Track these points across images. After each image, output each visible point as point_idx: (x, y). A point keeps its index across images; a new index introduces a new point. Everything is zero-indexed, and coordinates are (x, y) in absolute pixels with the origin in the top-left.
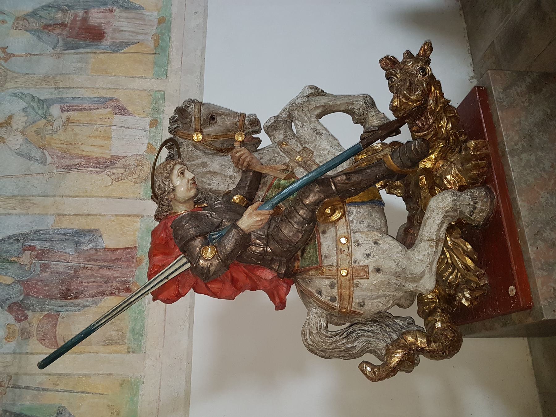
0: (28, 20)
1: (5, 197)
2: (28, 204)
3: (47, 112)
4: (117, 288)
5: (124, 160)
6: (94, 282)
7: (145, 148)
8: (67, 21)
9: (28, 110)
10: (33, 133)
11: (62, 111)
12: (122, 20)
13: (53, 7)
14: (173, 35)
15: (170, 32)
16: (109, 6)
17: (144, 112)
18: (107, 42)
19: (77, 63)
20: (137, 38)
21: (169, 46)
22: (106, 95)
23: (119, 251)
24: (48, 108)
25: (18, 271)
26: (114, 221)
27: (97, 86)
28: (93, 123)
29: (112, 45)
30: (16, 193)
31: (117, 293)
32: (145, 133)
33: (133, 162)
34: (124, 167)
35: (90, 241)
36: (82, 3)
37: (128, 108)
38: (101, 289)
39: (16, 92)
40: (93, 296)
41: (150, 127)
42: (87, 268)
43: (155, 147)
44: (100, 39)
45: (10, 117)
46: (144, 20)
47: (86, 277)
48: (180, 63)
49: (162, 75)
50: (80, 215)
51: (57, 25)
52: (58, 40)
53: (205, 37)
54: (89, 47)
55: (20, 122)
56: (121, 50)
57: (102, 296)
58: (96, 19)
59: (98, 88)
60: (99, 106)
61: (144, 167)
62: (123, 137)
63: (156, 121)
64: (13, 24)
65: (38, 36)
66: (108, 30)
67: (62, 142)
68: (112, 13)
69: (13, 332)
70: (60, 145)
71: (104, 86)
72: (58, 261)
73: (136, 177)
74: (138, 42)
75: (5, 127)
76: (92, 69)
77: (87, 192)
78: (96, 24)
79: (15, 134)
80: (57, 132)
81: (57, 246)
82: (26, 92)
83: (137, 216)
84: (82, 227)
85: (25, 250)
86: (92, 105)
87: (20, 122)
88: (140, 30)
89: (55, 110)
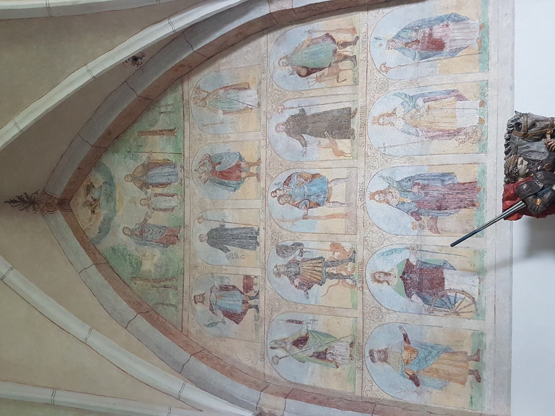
2: (413, 160)
5: (465, 130)
6: (454, 201)
7: (477, 121)
8: (419, 38)
10: (409, 118)
11: (424, 102)
12: (456, 31)
13: (409, 29)
14: (491, 36)
18: (447, 50)
20: (466, 44)
21: (489, 45)
23: (467, 184)
28: (444, 108)
29: (450, 52)
30: (405, 154)
32: (477, 111)
33: (470, 130)
34: (466, 134)
35: (450, 179)
38: (459, 205)
44: (442, 49)
45: (395, 110)
46: (470, 28)
48: (497, 58)
50: (442, 165)
53: (514, 34)
56: (457, 54)
58: (438, 34)
59: (444, 84)
61: (478, 133)
62: (464, 115)
64: (387, 45)
65: (403, 52)
66: (446, 41)
67: (427, 122)
68: (448, 27)
69: (416, 226)
70: (425, 124)
71: (448, 83)
75: (393, 116)
78: (438, 37)
83: (475, 163)
85: (414, 185)
86: (442, 96)
89: (420, 102)
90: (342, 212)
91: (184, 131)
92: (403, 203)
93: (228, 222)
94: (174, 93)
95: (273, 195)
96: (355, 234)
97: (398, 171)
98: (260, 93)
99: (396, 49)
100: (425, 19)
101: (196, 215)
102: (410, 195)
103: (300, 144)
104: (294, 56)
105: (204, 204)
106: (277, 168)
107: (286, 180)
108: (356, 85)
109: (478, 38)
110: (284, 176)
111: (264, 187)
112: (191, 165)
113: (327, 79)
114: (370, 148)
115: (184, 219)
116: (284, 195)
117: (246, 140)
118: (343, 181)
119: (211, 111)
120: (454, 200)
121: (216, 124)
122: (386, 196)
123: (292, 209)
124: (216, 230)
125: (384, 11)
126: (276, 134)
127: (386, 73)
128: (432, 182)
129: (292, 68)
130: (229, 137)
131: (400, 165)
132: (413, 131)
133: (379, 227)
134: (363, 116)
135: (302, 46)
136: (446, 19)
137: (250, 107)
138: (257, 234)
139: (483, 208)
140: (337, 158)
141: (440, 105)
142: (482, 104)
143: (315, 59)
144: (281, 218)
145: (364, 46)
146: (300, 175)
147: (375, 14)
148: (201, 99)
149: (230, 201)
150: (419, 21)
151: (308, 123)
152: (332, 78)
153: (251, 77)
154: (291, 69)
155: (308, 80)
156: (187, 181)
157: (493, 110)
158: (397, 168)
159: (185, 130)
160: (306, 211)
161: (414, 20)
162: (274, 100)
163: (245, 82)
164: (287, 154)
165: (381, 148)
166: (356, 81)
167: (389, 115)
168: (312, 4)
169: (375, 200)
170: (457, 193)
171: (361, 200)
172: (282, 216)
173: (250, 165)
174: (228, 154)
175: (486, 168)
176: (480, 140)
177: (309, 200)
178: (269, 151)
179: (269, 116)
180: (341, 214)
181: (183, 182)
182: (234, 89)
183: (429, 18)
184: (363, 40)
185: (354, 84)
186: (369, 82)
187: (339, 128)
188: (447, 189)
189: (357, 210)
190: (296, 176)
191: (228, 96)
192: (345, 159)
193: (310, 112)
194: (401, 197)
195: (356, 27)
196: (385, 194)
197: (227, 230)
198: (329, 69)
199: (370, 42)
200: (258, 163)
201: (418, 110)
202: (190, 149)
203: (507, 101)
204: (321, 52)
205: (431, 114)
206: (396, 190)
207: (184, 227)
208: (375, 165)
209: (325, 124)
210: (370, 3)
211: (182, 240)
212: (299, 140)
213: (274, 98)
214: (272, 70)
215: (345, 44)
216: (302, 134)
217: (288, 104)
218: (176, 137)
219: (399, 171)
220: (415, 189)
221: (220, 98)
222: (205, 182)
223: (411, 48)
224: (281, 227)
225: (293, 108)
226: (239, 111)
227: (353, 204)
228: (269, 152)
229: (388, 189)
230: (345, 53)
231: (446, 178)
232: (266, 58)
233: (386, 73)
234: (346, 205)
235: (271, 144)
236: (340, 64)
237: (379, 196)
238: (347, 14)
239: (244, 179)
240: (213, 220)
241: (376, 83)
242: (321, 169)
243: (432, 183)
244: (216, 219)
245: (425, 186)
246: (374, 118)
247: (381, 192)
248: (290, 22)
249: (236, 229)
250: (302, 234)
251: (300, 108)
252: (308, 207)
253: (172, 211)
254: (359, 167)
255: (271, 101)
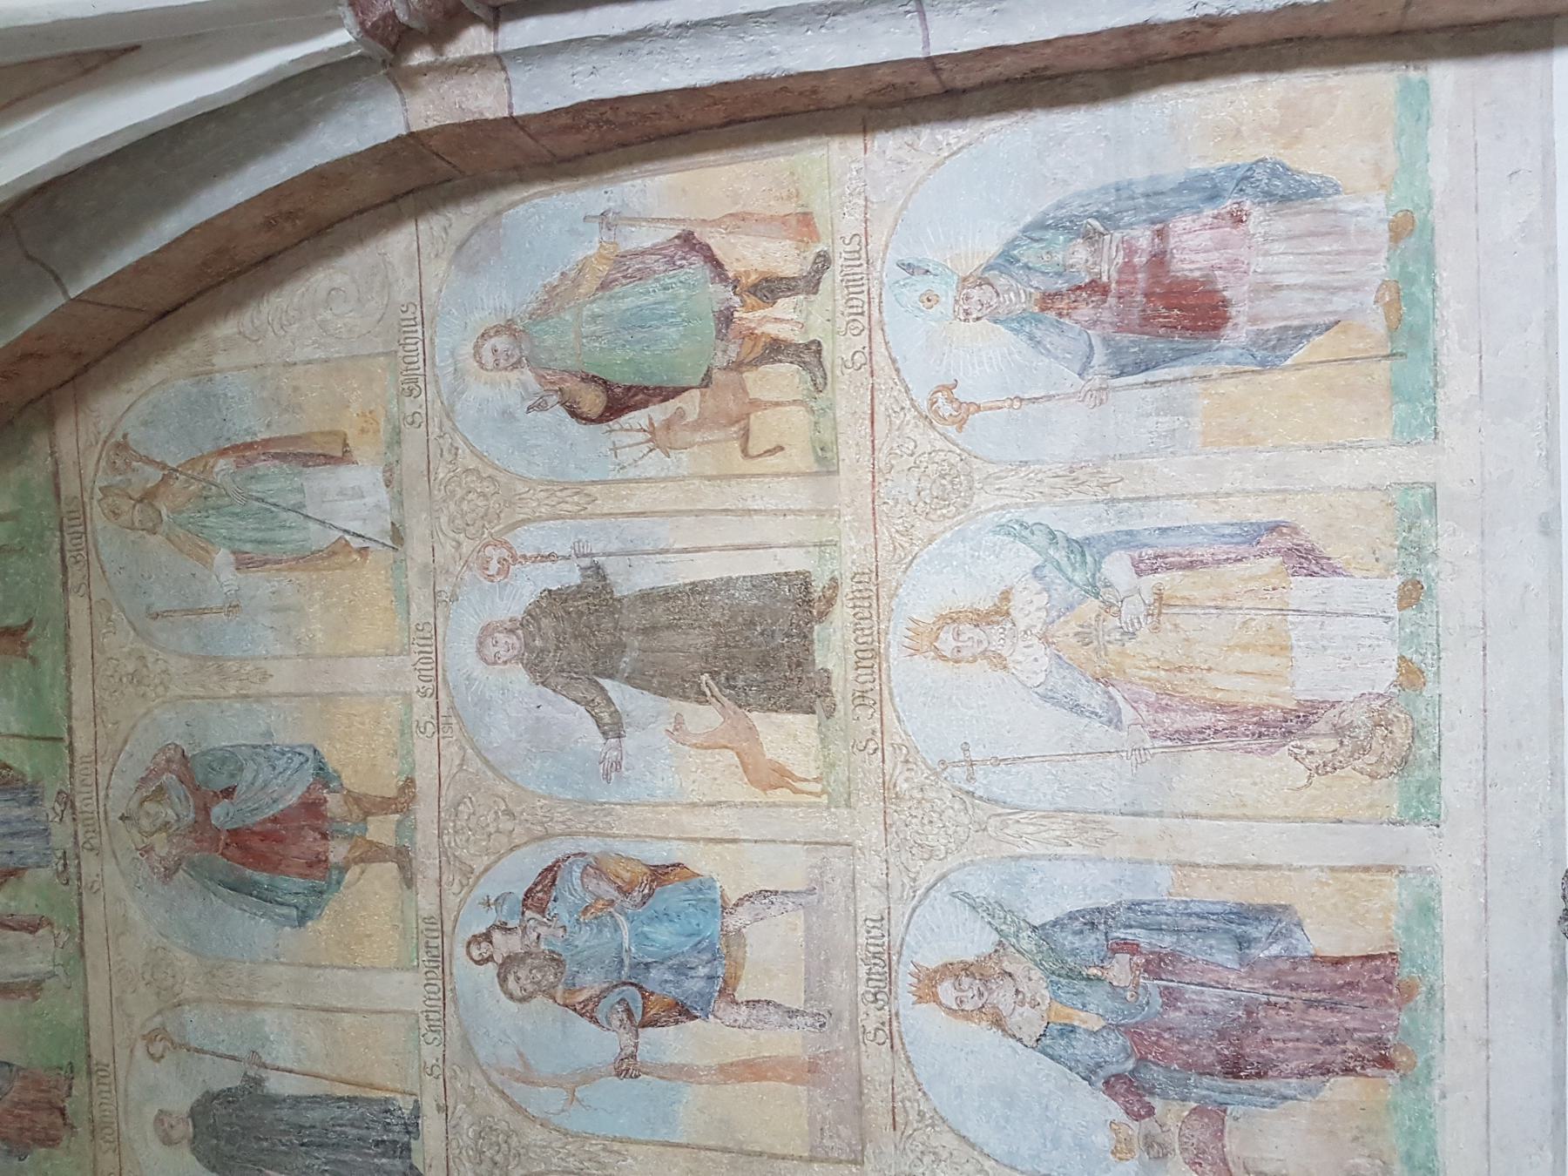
0: (992, 281)
1: (1038, 814)
2: (1099, 834)
3: (1098, 575)
4: (1358, 1057)
5: (1335, 711)
6: (1298, 1040)
7: (1391, 674)
8: (1107, 271)
9: (1046, 571)
10: (1073, 641)
11: (1139, 573)
12: (1278, 247)
13: (1056, 227)
14: (1444, 276)
15: (1435, 266)
16: (1230, 202)
17: (1377, 560)
18: (1237, 334)
19: (1158, 415)
20: (1330, 308)
21: (1435, 320)
22: (1258, 515)
23: (1352, 964)
24: (1097, 564)
25: (1109, 1002)
26: (1329, 885)
27: (1227, 486)
28: (1232, 604)
29: (1254, 343)
30: (1063, 804)
31: (1358, 1069)
32: (1386, 628)
33: (1359, 716)
34: (1338, 731)
35: (1274, 937)
36: (1142, 200)
37: (1328, 552)
38: (1319, 1059)
39: (1004, 521)
40: (1302, 1075)
41: (1401, 609)
42: (1275, 1004)
43: (1420, 670)
44: (1216, 328)
45: (1006, 596)
46: (1344, 233)
47: (1277, 1027)
48: (1476, 380)
49: (1422, 427)
50: (1237, 867)
51: (1078, 292)
52: (1091, 344)
53: (1552, 270)
54: (1185, 360)
55: (1033, 609)
56: (1286, 358)
57: (1322, 1074)
58: (1193, 257)
59: (1228, 495)
60: (1243, 549)
61: (1394, 729)
62: (1325, 643)
63: (1417, 584)
64: (956, 302)
65: (1031, 338)
66: (1235, 291)
67: (1154, 663)
68: (1242, 227)
69: (1128, 1141)
70: (1148, 673)
71: (1249, 487)
72: (1202, 985)
73: (1374, 759)
74: (1337, 323)
75: (998, 623)
76: (1203, 433)
77: (1244, 805)
78: (1197, 274)
79: (1026, 643)
80: (1134, 634)
81: (1190, 945)
82: (1030, 520)
83: (1388, 869)
84: (1247, 899)
85: (1115, 952)
86: (1221, 550)
87: (1033, 609)
88: (1336, 277)
89: (1117, 568)
90: (792, 1053)
91: (67, 636)
92: (1068, 1031)
93: (278, 1069)
94: (19, 463)
95: (475, 953)
96: (855, 1162)
97: (1034, 879)
98: (401, 483)
99: (1001, 322)
100: (1130, 183)
101: (138, 1021)
102: (1097, 997)
103: (591, 721)
104: (543, 326)
105: (169, 971)
106: (492, 829)
107: (536, 884)
108: (829, 473)
109: (1384, 282)
110: (522, 869)
111: (436, 913)
112: (102, 794)
113: (698, 438)
114: (907, 761)
115: (88, 1035)
116: (529, 954)
117: (343, 694)
118: (790, 906)
119: (181, 551)
120: (1298, 1035)
121: (203, 612)
122: (991, 991)
123: (564, 1024)
124: (226, 1097)
125: (939, 137)
126: (479, 670)
127: (960, 429)
128: (1194, 941)
129: (540, 378)
130: (265, 676)
131: (1041, 850)
132: (1093, 697)
133: (964, 1133)
134: (867, 615)
135: (576, 284)
136: (1230, 186)
137: (356, 543)
138: (408, 1133)
139: (1429, 1080)
140: (758, 796)
141: (1212, 592)
142: (1413, 594)
143: (638, 347)
144: (519, 1067)
145: (855, 303)
146: (597, 868)
147: (900, 153)
148: (137, 496)
149: (282, 968)
150: (1104, 189)
151: (622, 629)
152: (718, 434)
153: (355, 408)
154: (535, 386)
155: (614, 437)
156: (90, 866)
157: (1462, 627)
158: (1032, 864)
159: (72, 633)
160: (627, 1039)
161: (1079, 185)
162: (463, 515)
163: (327, 429)
164: (536, 766)
165: (954, 764)
166: (829, 455)
167: (982, 619)
168: (602, 102)
169: (940, 1004)
170: (1310, 1004)
171: (876, 1000)
172: (521, 1055)
173: (369, 807)
174: (264, 750)
175: (1439, 893)
176: (1405, 760)
177: (640, 988)
178: (455, 749)
179: (445, 587)
180: (788, 1062)
181: (72, 870)
182: (282, 457)
183: (1151, 178)
184: (848, 270)
185: (815, 468)
186: (882, 465)
187: (763, 663)
188: (1263, 980)
189: (863, 1048)
190: (577, 872)
191: (256, 488)
192: (796, 805)
193: (632, 579)
194: (1056, 1005)
195: (816, 208)
196: (985, 980)
197: (273, 1101)
198: (703, 395)
199: (882, 283)
200: (402, 801)
201: (1112, 605)
202: (98, 720)
203: (1527, 587)
204: (662, 317)
205: (1169, 627)
206: (1032, 966)
207: (89, 1073)
208: (932, 842)
209: (698, 641)
210: (870, 98)
211: (83, 1130)
212: (588, 704)
213: (465, 506)
214: (447, 380)
215: (769, 288)
216: (601, 681)
217: (528, 540)
218: (34, 661)
219: (1041, 880)
220: (1120, 970)
221: (220, 496)
222: (169, 873)
223: (1066, 320)
224: (518, 1108)
225: (551, 557)
226: (307, 559)
227: (840, 1019)
228: (451, 752)
229: (995, 957)
230: (772, 329)
231: (1259, 931)
232: (419, 328)
233: (960, 429)
234: (810, 1021)
235: (458, 716)
236: (750, 376)
237: (958, 986)
238: (769, 148)
239: (343, 869)
240: (214, 1054)
241: (916, 473)
242: (693, 845)
243: (1193, 947)
244: (222, 1049)
245: (1161, 960)
246: (912, 625)
247: (967, 968)
248: (516, 168)
249: (316, 1100)
250: (617, 1146)
251: (586, 562)
252: (638, 1018)
253: (36, 998)
254: (859, 843)
255: (452, 520)
